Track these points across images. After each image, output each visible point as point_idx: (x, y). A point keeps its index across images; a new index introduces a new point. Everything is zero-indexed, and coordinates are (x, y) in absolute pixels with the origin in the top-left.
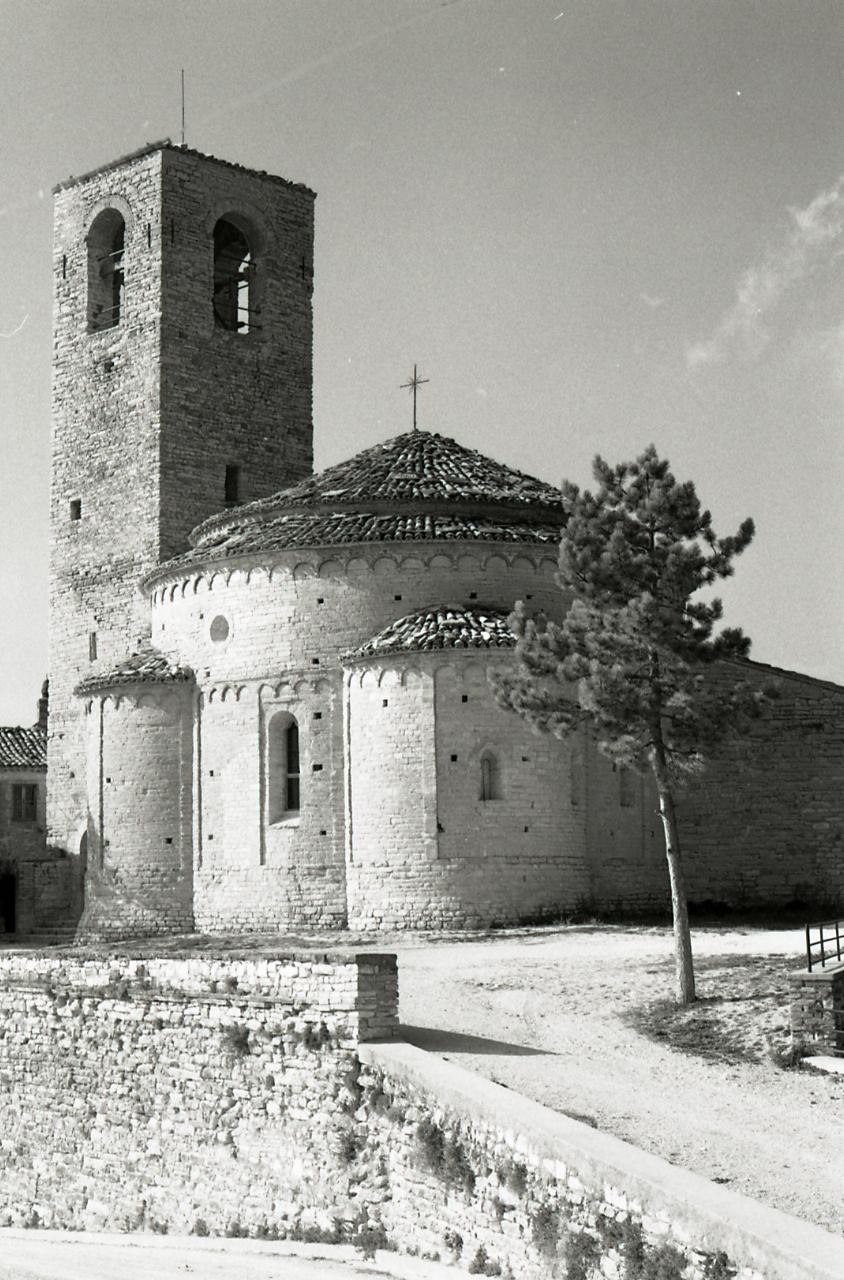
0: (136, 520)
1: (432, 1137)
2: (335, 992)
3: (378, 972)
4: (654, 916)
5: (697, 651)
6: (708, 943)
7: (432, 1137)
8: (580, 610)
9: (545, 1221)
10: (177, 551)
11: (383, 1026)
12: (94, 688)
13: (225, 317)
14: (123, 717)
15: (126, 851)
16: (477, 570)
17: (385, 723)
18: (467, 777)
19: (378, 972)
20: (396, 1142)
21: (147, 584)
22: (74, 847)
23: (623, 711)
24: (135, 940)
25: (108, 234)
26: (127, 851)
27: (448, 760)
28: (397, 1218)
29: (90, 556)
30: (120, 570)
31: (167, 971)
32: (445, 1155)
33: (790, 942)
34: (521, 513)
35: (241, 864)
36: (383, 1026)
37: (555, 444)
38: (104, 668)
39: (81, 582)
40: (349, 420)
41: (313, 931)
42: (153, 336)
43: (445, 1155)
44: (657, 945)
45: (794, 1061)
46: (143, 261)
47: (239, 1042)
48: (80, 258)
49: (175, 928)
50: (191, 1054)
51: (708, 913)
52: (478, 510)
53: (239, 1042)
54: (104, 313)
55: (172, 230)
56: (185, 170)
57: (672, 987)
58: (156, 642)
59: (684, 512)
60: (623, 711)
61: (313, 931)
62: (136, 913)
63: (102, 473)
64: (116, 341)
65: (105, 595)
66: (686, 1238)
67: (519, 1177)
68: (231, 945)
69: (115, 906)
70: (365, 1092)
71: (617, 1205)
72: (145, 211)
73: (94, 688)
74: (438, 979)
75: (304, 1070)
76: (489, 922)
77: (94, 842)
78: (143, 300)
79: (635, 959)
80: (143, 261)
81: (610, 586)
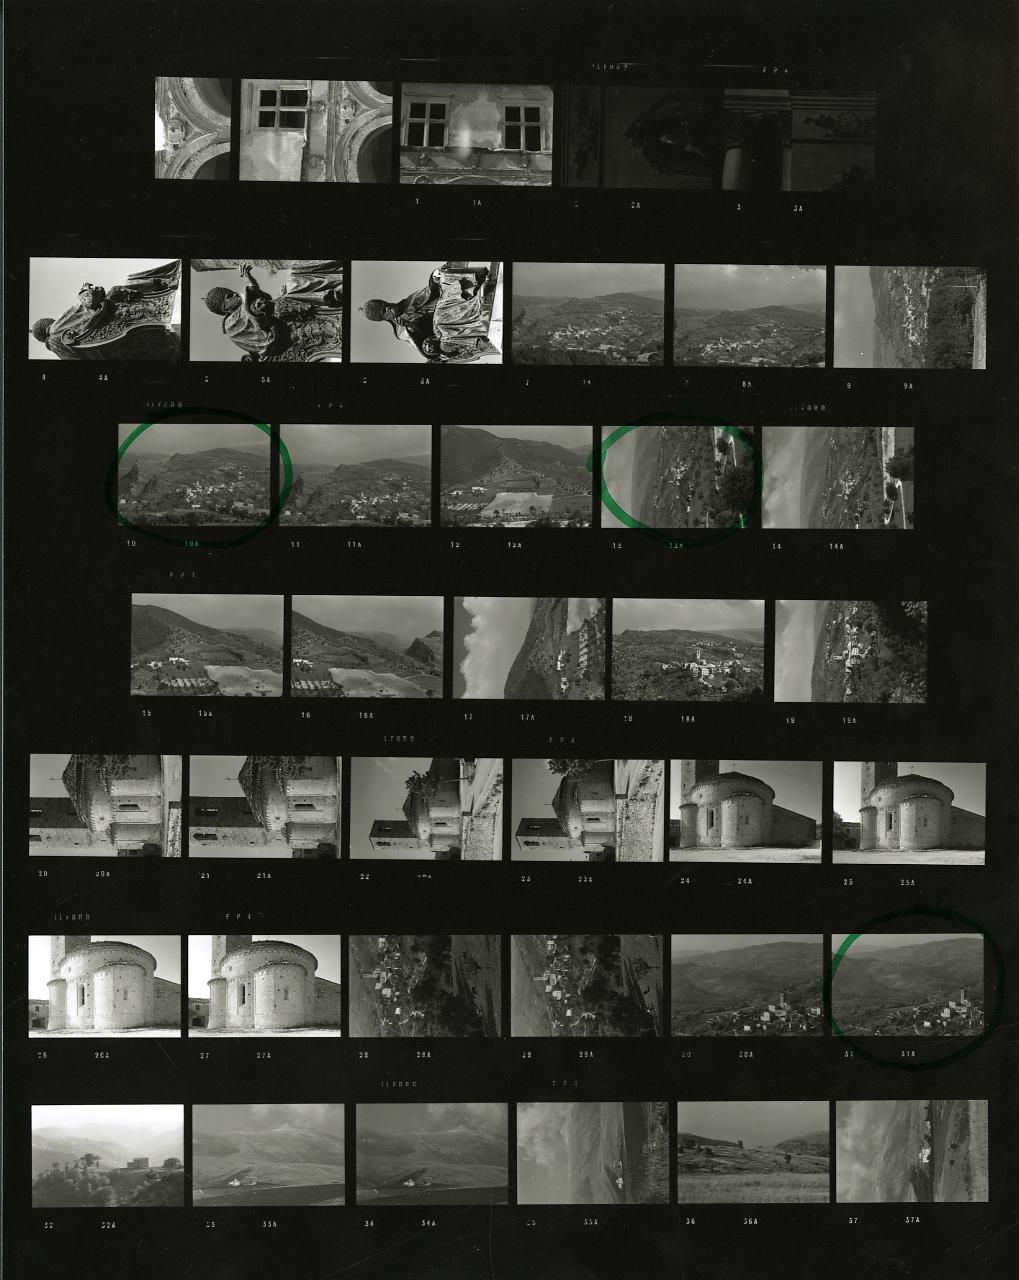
0: (563, 840)
1: (483, 808)
2: (466, 819)
3: (464, 814)
4: (459, 782)
5: (428, 778)
6: (462, 777)
7: (483, 808)
8: (424, 791)
9: (493, 795)
10: (566, 834)
11: (470, 813)
12: (583, 845)
13: (537, 829)
14: (434, 842)
15: (450, 842)
16: (418, 803)
17: (587, 807)
18: (442, 804)
19: (464, 814)
20: (484, 812)
21: (92, 831)
22: (317, 844)
23: (434, 786)
24: (460, 841)
25: (379, 844)
26: (145, 836)
27: (593, 798)
28: (492, 812)
29: (261, 840)
30: (264, 835)
31: (464, 838)
32: (485, 807)
33: (461, 767)
34: (412, 798)
35: (452, 829)
36: (470, 813)
37: (404, 793)
38: (285, 839)
39: (571, 847)
40: (401, 817)
41: (460, 821)
42: (42, 829)
43: (485, 807)
44: (462, 782)
45: (475, 767)
46: (382, 840)
47: (472, 829)
48: (204, 842)
49: (613, 834)
50: (474, 835)
51: (458, 777)
52: (561, 797)
53: (472, 829)
54: (388, 844)
55: (380, 837)
56: (372, 835)
57: (467, 781)
58: (104, 829)
59: (412, 779)
60: (434, 786)
61: (460, 821)
62: (157, 835)
63: (69, 839)
64: (392, 843)
65: (93, 838)
66: (495, 779)
67: (488, 798)
68: (461, 830)
69: (155, 838)
70: (478, 815)
71: (491, 787)
72: (377, 839)
73: (288, 841)
74: (465, 807)
75: (475, 822)
76: (459, 801)
77: (318, 840)
78: (387, 840)
79: (463, 785)
80: (382, 840)
81: (420, 787)
